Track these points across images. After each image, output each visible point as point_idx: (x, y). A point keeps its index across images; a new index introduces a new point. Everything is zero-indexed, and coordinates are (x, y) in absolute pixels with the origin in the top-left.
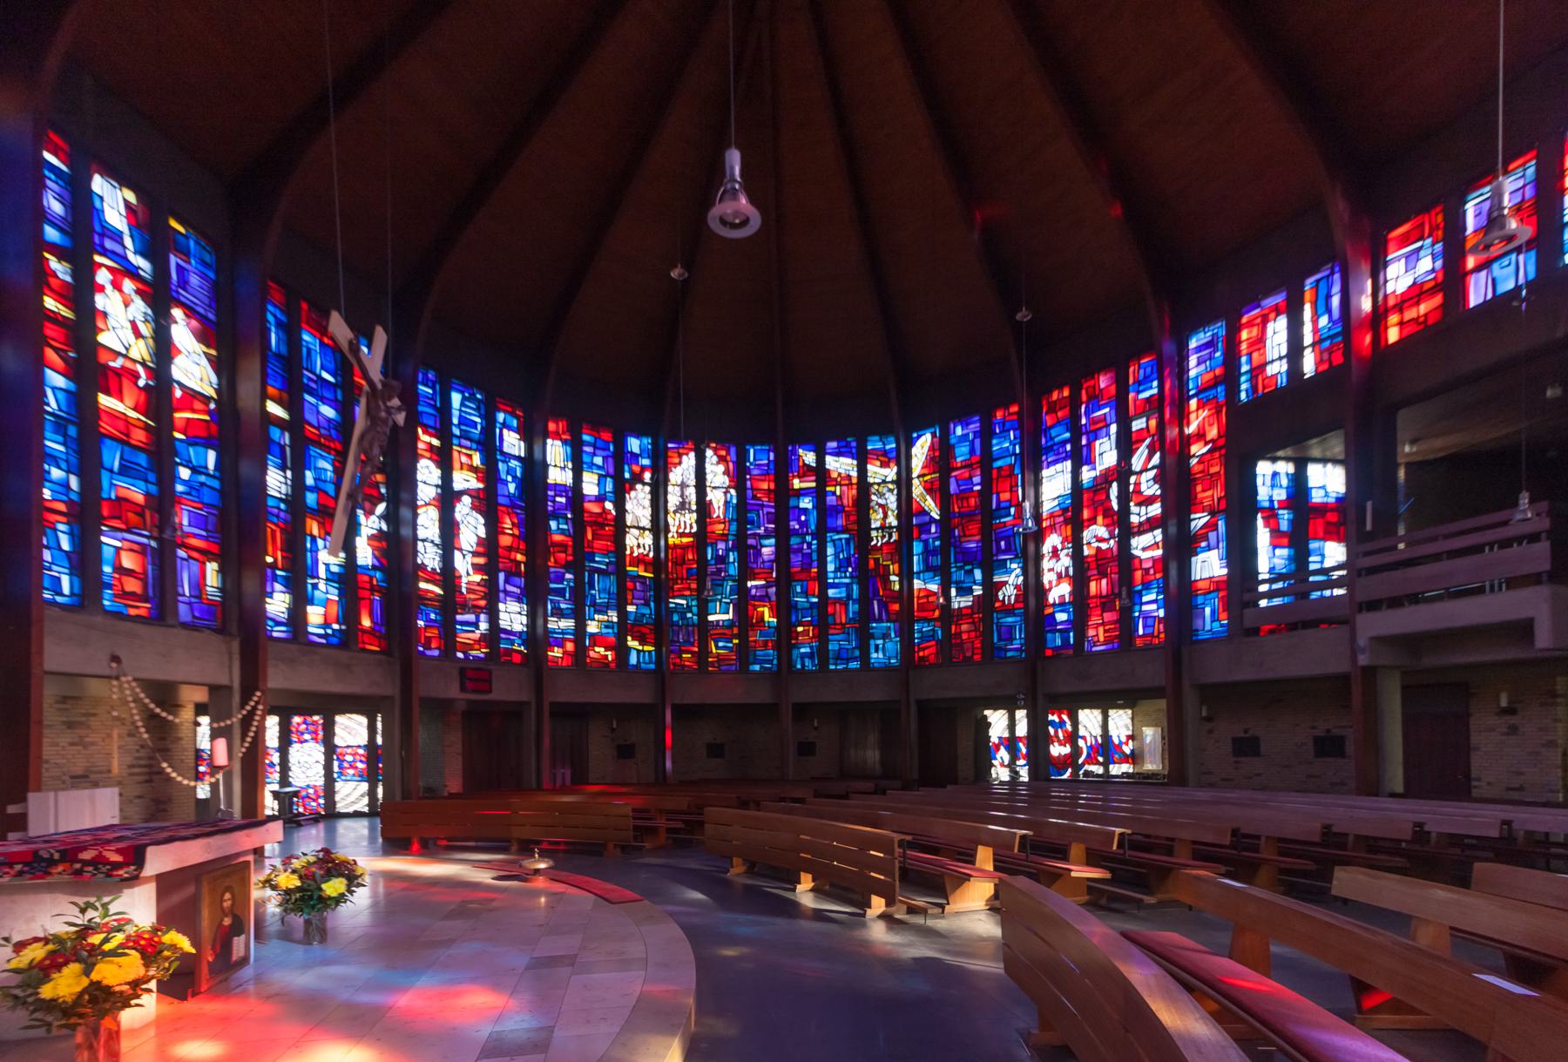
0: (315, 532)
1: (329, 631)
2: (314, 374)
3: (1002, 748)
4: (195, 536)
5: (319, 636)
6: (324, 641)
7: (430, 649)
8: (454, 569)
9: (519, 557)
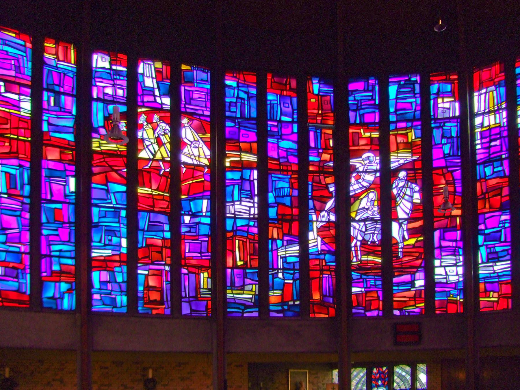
0: (275, 236)
1: (286, 307)
2: (276, 121)
3: (140, 258)
4: (193, 258)
5: (278, 311)
6: (281, 315)
7: (370, 310)
8: (391, 237)
9: (456, 212)
